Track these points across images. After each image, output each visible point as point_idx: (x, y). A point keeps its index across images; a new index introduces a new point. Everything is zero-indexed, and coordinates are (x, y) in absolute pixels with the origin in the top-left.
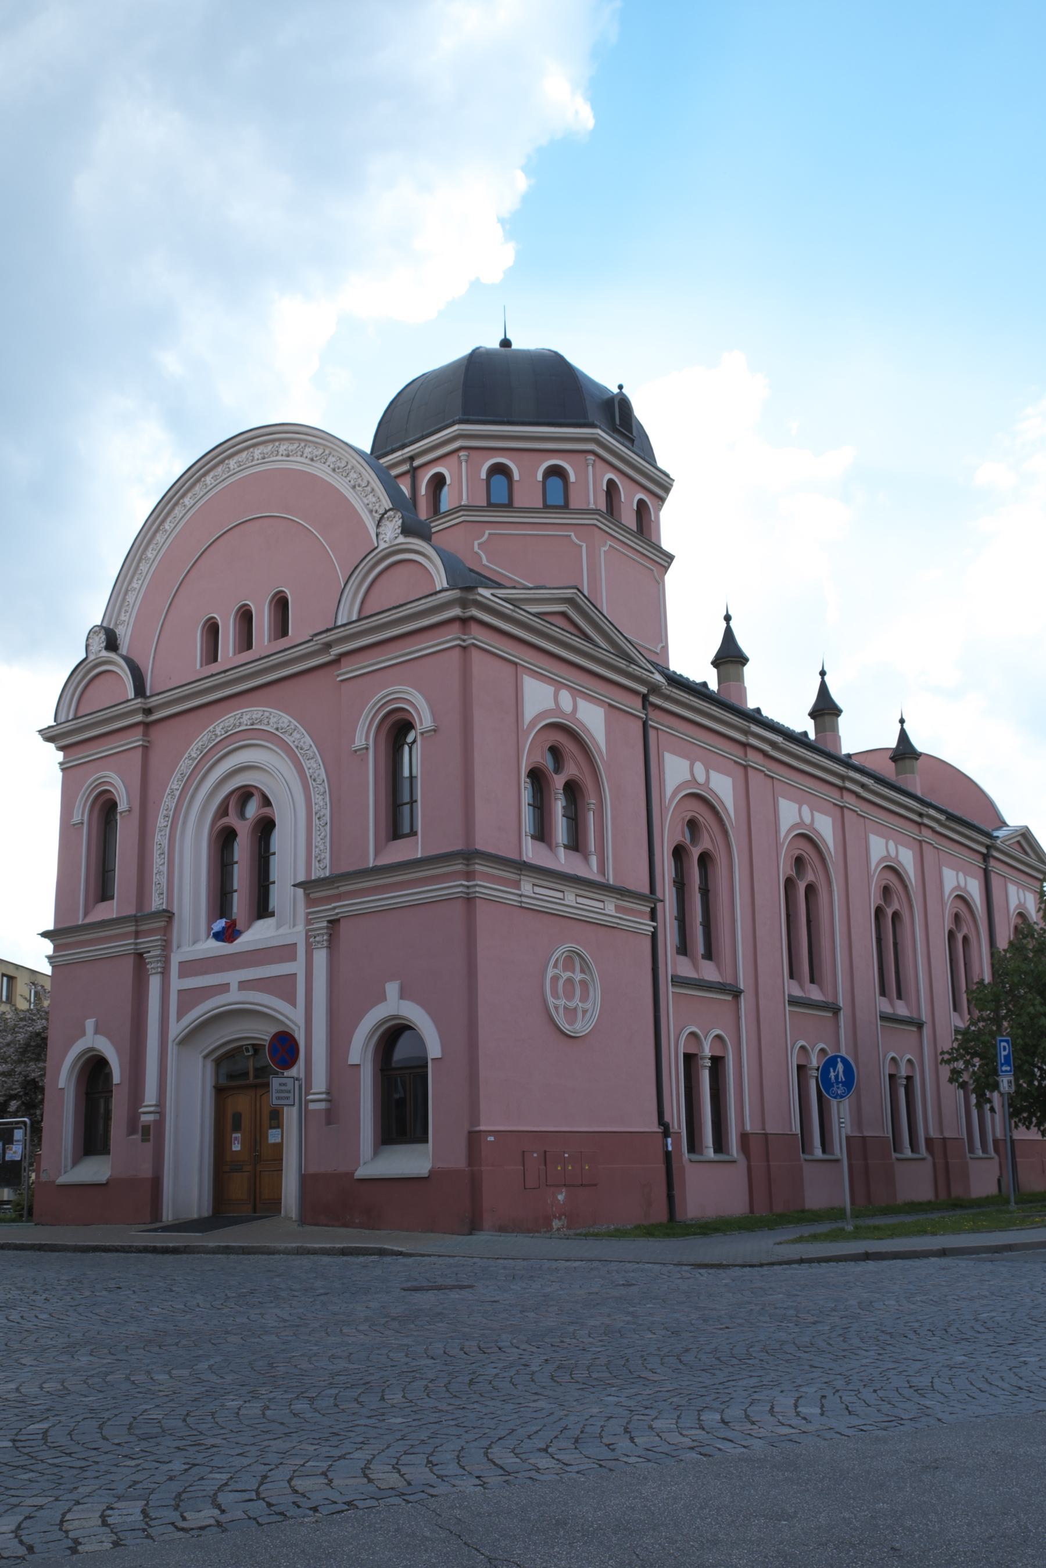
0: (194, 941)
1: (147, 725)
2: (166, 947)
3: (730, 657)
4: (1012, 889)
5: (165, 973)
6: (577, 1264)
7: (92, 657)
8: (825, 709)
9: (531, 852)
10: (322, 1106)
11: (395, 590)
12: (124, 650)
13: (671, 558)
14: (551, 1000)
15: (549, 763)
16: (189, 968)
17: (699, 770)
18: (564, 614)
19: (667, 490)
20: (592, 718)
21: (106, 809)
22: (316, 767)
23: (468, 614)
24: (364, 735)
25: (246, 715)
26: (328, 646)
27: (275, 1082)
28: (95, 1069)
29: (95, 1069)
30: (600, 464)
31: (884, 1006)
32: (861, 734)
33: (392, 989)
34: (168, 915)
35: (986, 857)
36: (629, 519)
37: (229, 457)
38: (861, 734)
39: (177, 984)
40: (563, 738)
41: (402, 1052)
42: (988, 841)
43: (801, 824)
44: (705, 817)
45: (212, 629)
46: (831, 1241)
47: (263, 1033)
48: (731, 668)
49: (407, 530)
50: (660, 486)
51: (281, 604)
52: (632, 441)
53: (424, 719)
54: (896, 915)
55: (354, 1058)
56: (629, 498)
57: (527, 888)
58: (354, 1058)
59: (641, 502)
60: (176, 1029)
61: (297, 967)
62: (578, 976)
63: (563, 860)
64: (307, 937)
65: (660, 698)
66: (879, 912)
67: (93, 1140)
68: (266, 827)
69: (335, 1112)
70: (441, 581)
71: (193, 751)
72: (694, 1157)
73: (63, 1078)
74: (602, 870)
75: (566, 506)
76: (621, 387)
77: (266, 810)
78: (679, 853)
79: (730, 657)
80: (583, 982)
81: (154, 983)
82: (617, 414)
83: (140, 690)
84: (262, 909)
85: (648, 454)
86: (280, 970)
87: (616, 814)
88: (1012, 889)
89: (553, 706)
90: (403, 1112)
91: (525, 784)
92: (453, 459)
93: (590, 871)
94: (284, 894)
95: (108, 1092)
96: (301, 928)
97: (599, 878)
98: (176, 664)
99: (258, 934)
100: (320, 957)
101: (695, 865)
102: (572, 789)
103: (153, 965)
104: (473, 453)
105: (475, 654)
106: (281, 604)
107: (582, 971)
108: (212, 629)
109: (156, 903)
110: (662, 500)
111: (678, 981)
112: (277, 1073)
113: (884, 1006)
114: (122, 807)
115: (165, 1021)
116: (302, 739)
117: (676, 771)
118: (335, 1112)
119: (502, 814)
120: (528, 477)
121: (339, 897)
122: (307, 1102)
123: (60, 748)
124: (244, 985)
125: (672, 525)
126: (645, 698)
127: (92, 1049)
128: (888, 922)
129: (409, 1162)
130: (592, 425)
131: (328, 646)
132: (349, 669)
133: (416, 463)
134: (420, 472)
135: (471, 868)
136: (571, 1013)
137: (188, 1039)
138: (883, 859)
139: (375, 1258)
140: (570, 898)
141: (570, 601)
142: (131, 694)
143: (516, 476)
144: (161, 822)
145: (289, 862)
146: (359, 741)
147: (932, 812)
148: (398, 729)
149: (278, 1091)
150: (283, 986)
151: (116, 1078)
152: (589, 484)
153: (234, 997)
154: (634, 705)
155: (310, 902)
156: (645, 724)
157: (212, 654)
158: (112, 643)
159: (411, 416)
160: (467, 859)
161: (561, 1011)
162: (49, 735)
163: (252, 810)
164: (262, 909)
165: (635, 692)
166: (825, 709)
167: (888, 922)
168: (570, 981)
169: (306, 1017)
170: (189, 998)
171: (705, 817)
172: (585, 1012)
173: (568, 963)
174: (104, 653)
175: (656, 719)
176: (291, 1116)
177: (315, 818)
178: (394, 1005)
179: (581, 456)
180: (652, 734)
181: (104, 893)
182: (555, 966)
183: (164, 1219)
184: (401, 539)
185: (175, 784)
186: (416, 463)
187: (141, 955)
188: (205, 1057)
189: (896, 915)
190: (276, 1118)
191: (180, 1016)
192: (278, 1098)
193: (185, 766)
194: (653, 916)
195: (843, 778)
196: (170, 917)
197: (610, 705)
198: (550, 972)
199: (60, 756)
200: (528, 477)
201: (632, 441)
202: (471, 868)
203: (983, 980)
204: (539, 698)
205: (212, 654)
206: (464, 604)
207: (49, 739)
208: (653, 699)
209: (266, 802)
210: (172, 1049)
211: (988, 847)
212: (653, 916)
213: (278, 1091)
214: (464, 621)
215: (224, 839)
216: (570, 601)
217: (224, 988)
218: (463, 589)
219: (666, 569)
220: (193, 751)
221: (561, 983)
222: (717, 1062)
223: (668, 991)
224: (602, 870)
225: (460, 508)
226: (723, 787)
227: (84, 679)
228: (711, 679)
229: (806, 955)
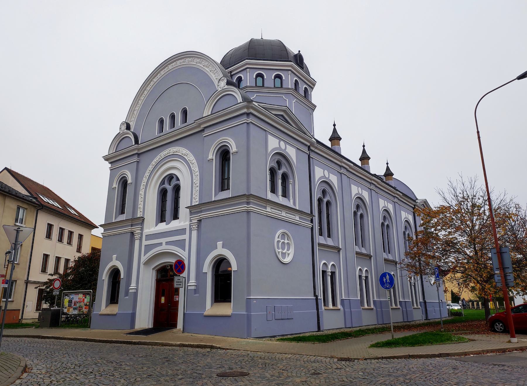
0: (151, 226)
1: (139, 155)
2: (142, 229)
3: (335, 138)
4: (270, 137)
5: (141, 239)
6: (290, 356)
7: (121, 132)
8: (365, 158)
9: (270, 196)
10: (193, 288)
11: (224, 104)
12: (132, 130)
13: (315, 106)
14: (277, 250)
15: (275, 165)
16: (149, 237)
17: (326, 172)
18: (282, 116)
19: (314, 85)
20: (291, 152)
21: (124, 183)
22: (196, 168)
23: (249, 112)
24: (212, 155)
25: (172, 150)
26: (200, 125)
27: (176, 278)
28: (115, 274)
29: (115, 274)
30: (292, 74)
31: (385, 256)
32: (377, 168)
33: (220, 244)
34: (142, 219)
35: (414, 208)
36: (302, 92)
37: (169, 64)
38: (377, 168)
39: (145, 243)
40: (281, 158)
41: (222, 268)
42: (414, 203)
43: (358, 194)
44: (328, 189)
45: (162, 121)
46: (395, 347)
47: (173, 260)
48: (336, 141)
49: (229, 83)
50: (312, 84)
51: (185, 112)
52: (303, 69)
53: (233, 148)
54: (388, 226)
55: (205, 270)
56: (302, 87)
57: (269, 209)
58: (205, 270)
59: (306, 88)
60: (144, 259)
61: (186, 237)
62: (286, 241)
63: (281, 200)
64: (190, 226)
65: (312, 148)
66: (383, 224)
67: (113, 299)
68: (177, 189)
69: (199, 289)
70: (240, 100)
71: (154, 163)
72: (326, 308)
73: (104, 277)
74: (294, 204)
75: (282, 87)
76: (299, 51)
77: (178, 182)
78: (320, 200)
79: (335, 138)
80: (288, 243)
81: (137, 242)
82: (299, 59)
83: (137, 142)
84: (176, 216)
85: (308, 73)
86: (178, 237)
87: (298, 185)
88: (270, 137)
89: (278, 146)
90: (223, 290)
91: (268, 172)
92: (245, 72)
93: (291, 204)
94: (183, 211)
95: (119, 283)
96: (188, 223)
97: (294, 207)
98: (149, 133)
99: (175, 225)
100: (194, 233)
101: (323, 206)
102: (285, 177)
103: (137, 236)
104: (251, 70)
105: (251, 125)
106: (185, 112)
107: (288, 240)
108: (162, 121)
109: (139, 215)
110: (312, 88)
111: (320, 245)
112: (177, 275)
113: (385, 256)
114: (129, 181)
115: (140, 256)
116: (191, 158)
117: (319, 173)
118: (199, 289)
119: (261, 185)
120: (269, 78)
121: (201, 212)
122: (188, 286)
123: (111, 163)
124: (167, 243)
125: (315, 96)
126: (309, 147)
127: (114, 266)
128: (385, 228)
129: (225, 309)
130: (291, 61)
131: (200, 125)
132: (207, 133)
133: (232, 74)
134: (233, 77)
135: (249, 201)
136: (284, 255)
137: (147, 263)
138: (383, 207)
139: (209, 350)
140: (284, 214)
141: (284, 111)
142: (134, 144)
143: (265, 77)
144: (142, 187)
145: (184, 201)
146: (210, 157)
147: (398, 192)
148: (224, 155)
149: (177, 282)
150: (181, 244)
151: (122, 276)
152: (289, 81)
153: (164, 248)
154: (306, 150)
155: (191, 213)
156: (309, 157)
157: (161, 129)
158: (128, 127)
159: (230, 61)
160: (248, 197)
161: (280, 253)
162: (106, 159)
163: (174, 182)
164: (176, 216)
165: (306, 145)
166: (365, 158)
167: (385, 228)
168: (283, 243)
169: (188, 255)
170: (149, 248)
171: (328, 189)
172: (289, 254)
173: (283, 235)
174: (125, 131)
175: (312, 155)
176: (181, 291)
177: (194, 185)
178: (220, 250)
179: (287, 72)
180: (311, 159)
181: (122, 212)
182: (278, 238)
183: (136, 328)
184: (226, 87)
185: (147, 174)
186: (232, 74)
187: (132, 233)
188: (153, 269)
189: (388, 226)
190: (177, 291)
191: (145, 253)
192: (177, 285)
193: (151, 168)
194: (312, 221)
195: (371, 179)
196: (143, 220)
197: (298, 148)
198: (276, 239)
199: (110, 165)
200: (269, 78)
201: (303, 69)
202: (249, 201)
203: (133, 316)
204: (274, 143)
205: (161, 129)
206: (248, 107)
207: (106, 160)
208: (312, 148)
209: (178, 179)
210: (142, 266)
211: (414, 205)
212: (312, 221)
213: (177, 282)
214: (248, 114)
215: (163, 193)
216: (284, 111)
217: (161, 244)
218: (247, 102)
219: (314, 110)
220: (154, 163)
221: (280, 243)
222: (333, 273)
223: (317, 248)
224: (294, 204)
225: (247, 87)
226: (334, 179)
227: (119, 139)
228: (329, 144)
229: (361, 238)
